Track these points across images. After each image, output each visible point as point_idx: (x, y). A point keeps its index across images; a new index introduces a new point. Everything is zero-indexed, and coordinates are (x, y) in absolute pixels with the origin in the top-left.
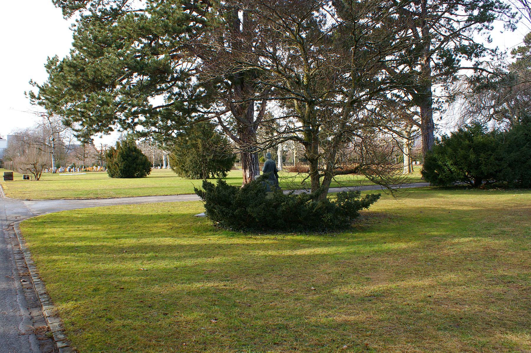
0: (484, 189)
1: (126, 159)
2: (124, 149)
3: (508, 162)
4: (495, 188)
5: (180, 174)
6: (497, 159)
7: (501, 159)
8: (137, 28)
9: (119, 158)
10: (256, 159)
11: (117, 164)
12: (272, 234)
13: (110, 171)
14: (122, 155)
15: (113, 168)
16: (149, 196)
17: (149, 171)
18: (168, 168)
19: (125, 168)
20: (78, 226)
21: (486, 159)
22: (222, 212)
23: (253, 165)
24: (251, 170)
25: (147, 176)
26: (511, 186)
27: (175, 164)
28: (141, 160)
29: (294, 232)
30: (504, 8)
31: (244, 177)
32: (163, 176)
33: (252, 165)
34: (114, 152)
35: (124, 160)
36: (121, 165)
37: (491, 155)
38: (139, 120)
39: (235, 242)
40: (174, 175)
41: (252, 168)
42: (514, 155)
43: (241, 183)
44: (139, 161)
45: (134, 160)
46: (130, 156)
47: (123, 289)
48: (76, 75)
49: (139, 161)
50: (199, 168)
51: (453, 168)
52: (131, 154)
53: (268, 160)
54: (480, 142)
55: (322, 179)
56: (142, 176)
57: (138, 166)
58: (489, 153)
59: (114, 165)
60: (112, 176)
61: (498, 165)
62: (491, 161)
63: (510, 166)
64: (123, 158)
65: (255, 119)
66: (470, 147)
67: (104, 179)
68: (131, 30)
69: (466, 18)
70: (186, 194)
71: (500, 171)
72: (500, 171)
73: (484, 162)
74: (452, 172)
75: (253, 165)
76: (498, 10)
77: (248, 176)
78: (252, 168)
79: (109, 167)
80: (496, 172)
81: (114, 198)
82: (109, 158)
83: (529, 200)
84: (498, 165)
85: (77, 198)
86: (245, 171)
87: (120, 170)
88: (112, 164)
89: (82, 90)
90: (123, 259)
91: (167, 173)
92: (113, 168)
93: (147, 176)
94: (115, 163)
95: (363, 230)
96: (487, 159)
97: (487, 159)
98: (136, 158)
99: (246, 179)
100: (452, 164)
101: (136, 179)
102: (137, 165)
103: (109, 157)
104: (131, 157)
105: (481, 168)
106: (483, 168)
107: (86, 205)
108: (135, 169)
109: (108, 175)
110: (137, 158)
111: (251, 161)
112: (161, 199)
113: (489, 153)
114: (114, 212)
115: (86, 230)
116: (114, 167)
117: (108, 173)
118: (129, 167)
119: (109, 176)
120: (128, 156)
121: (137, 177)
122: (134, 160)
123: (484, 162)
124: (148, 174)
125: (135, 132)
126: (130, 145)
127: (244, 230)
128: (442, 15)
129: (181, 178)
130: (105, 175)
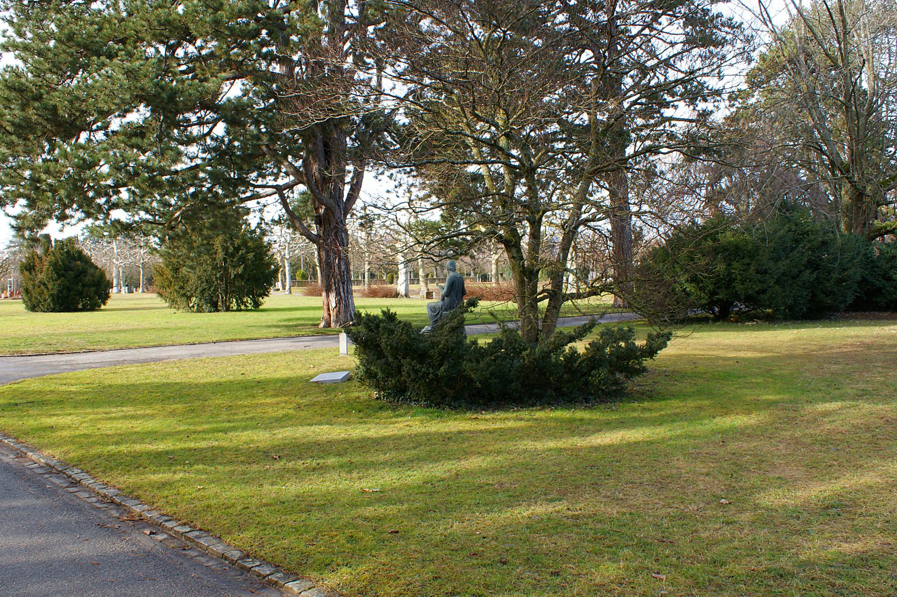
0: (737, 321)
1: (63, 275)
2: (58, 255)
3: (775, 277)
4: (754, 321)
5: (173, 303)
6: (758, 272)
7: (765, 272)
8: (156, 23)
9: (50, 272)
10: (347, 272)
11: (44, 284)
12: (569, 408)
13: (30, 299)
14: (55, 265)
15: (35, 293)
16: (160, 346)
17: (105, 297)
18: (123, 292)
19: (60, 291)
20: (107, 410)
21: (741, 272)
22: (416, 372)
23: (343, 283)
24: (338, 294)
25: (103, 307)
26: (779, 316)
27: (166, 284)
28: (93, 276)
29: (538, 404)
30: (733, 27)
31: (326, 307)
32: (132, 306)
33: (341, 284)
34: (37, 261)
35: (59, 276)
36: (53, 287)
37: (749, 264)
38: (119, 198)
39: (467, 428)
40: (159, 306)
41: (341, 290)
42: (783, 265)
43: (319, 319)
44: (88, 279)
45: (79, 275)
46: (71, 269)
47: (397, 532)
48: (23, 107)
49: (88, 279)
50: (214, 290)
51: (689, 287)
52: (72, 265)
53: (451, 274)
54: (729, 243)
55: (544, 304)
56: (93, 307)
57: (86, 288)
58: (747, 261)
59: (39, 287)
60: (33, 308)
61: (760, 281)
62: (751, 275)
63: (776, 282)
64: (56, 273)
65: (345, 199)
66: (716, 251)
67: (17, 313)
68: (144, 26)
69: (682, 38)
70: (241, 340)
71: (764, 291)
72: (764, 291)
73: (739, 277)
74: (688, 294)
75: (343, 283)
76: (726, 29)
77: (334, 305)
78: (341, 290)
79: (27, 291)
80: (758, 293)
81: (94, 351)
82: (27, 273)
83: (892, 337)
84: (760, 281)
85: (17, 352)
86: (328, 296)
87: (52, 295)
88: (34, 285)
89: (31, 137)
90: (320, 470)
91: (136, 302)
92: (35, 293)
93: (103, 307)
94: (40, 282)
95: (651, 396)
96: (743, 271)
97: (743, 271)
98: (81, 273)
99: (329, 309)
100: (687, 281)
101: (79, 313)
102: (84, 286)
103: (27, 270)
104: (73, 271)
105: (734, 287)
106: (739, 287)
107: (74, 367)
108: (81, 294)
109: (24, 305)
110: (84, 272)
111: (339, 277)
112: (199, 352)
113: (747, 261)
114: (120, 380)
115: (132, 417)
116: (38, 290)
117: (25, 302)
118: (69, 290)
119: (28, 308)
120: (67, 268)
121: (84, 309)
122: (79, 275)
123: (739, 277)
124: (104, 304)
125: (109, 222)
126: (69, 247)
127: (450, 406)
128: (643, 29)
129: (173, 310)
130: (19, 306)
